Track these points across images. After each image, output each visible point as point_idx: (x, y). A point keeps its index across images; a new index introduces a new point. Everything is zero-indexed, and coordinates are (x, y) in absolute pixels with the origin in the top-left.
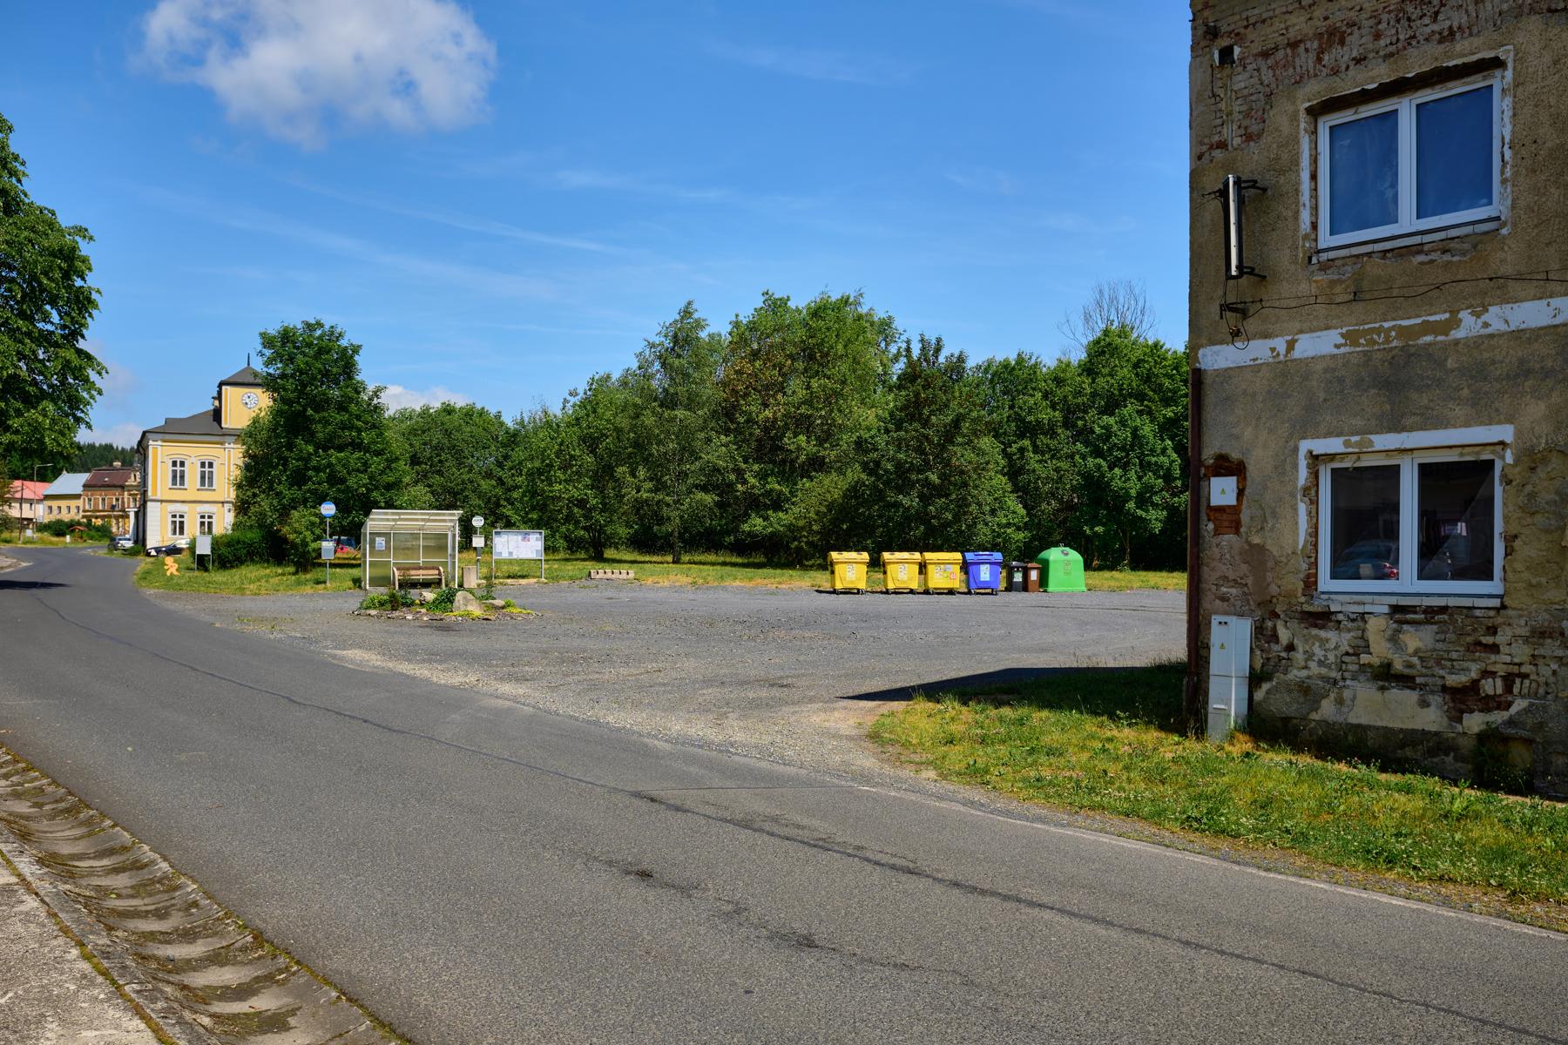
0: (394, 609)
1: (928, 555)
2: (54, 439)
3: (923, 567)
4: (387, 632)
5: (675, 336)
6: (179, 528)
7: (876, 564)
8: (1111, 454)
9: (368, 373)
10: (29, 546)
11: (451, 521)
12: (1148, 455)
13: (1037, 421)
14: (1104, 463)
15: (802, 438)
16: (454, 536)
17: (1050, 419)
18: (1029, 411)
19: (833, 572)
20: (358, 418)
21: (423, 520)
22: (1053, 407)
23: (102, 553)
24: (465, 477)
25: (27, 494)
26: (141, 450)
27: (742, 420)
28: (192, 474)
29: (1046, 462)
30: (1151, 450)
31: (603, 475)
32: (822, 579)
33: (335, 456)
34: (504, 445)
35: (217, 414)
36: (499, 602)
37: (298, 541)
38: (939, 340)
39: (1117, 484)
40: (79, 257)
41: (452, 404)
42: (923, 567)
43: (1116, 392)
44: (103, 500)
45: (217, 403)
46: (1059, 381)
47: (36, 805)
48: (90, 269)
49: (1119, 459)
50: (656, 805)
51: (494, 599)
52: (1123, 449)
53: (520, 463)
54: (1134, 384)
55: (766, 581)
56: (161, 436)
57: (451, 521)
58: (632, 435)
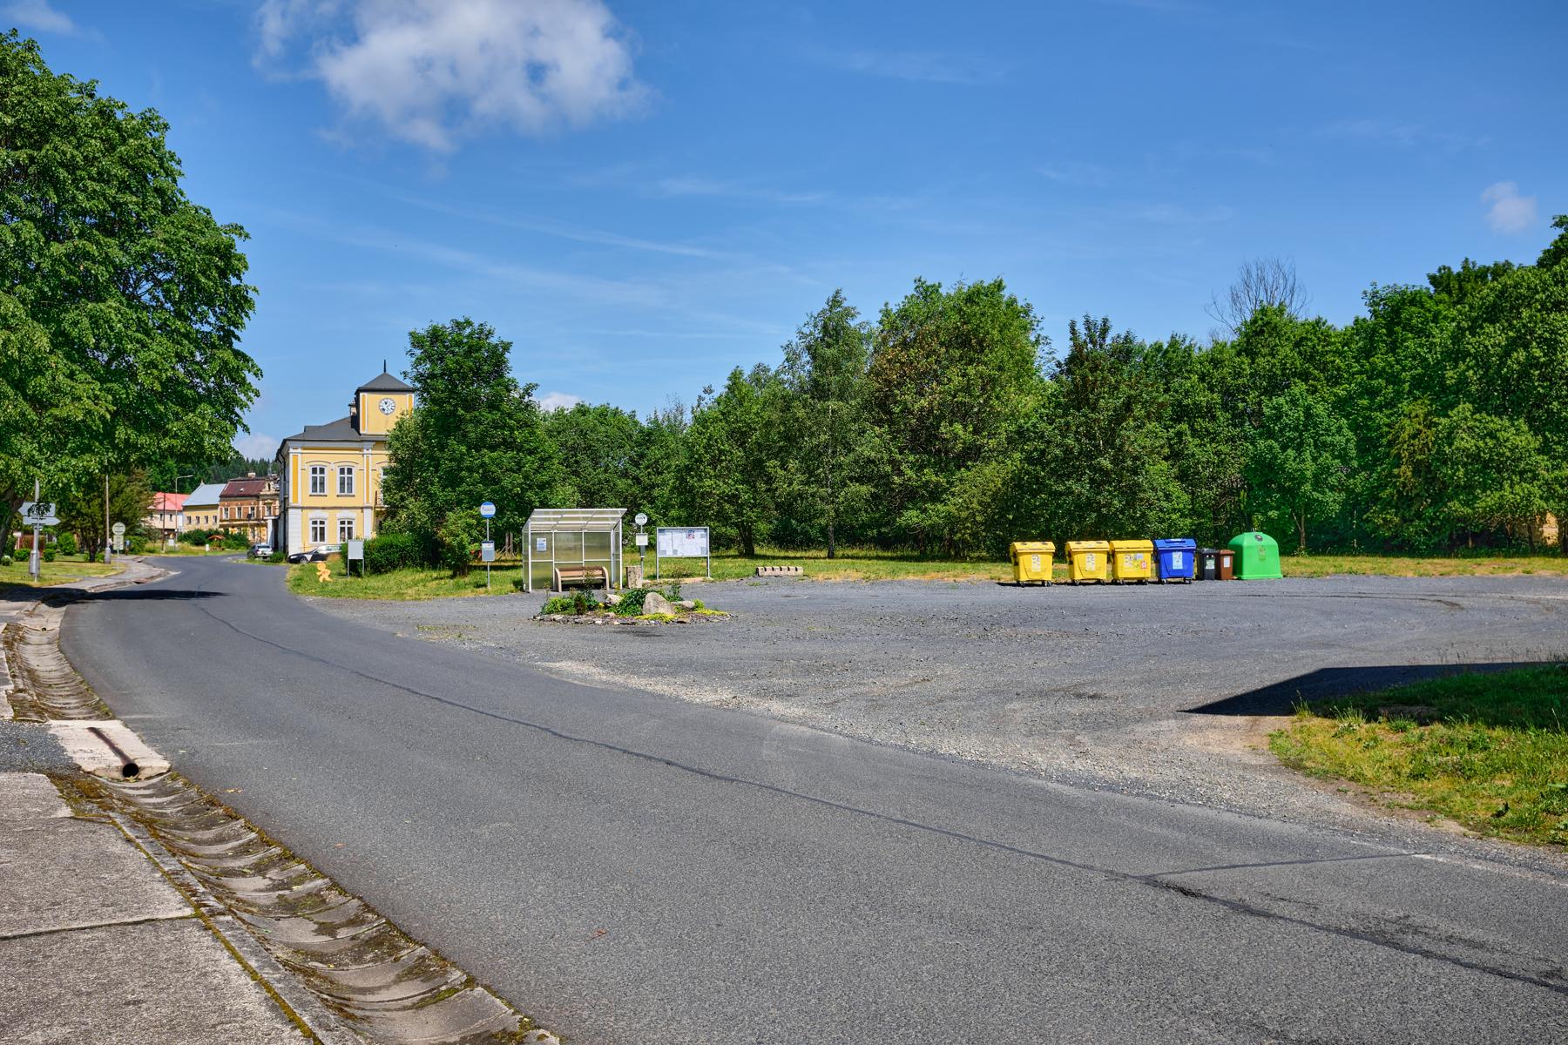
0: (580, 613)
1: (1117, 544)
2: (213, 443)
3: (1111, 556)
4: (583, 638)
5: (825, 327)
6: (320, 534)
7: (1061, 555)
8: (1283, 435)
9: (519, 371)
10: (171, 555)
11: (613, 519)
12: (1322, 435)
13: (1194, 404)
14: (1275, 445)
15: (958, 427)
16: (617, 534)
17: (1208, 402)
18: (1186, 395)
19: (1017, 564)
20: (510, 416)
21: (584, 519)
22: (1211, 390)
23: (243, 560)
24: (602, 477)
25: (169, 506)
26: (281, 458)
27: (897, 410)
28: (332, 480)
29: (1205, 446)
30: (1326, 430)
31: (754, 471)
32: (1003, 571)
33: (487, 456)
34: (639, 445)
35: (355, 421)
36: (689, 603)
37: (455, 543)
38: (1105, 321)
39: (1291, 465)
40: (235, 255)
41: (587, 404)
42: (1111, 556)
43: (1279, 372)
44: (239, 509)
45: (354, 410)
46: (1216, 363)
47: (324, 929)
48: (246, 268)
49: (1292, 440)
50: (672, 768)
51: (682, 600)
52: (1296, 429)
53: (657, 462)
54: (1298, 363)
55: (940, 575)
56: (301, 443)
57: (613, 519)
58: (782, 429)
